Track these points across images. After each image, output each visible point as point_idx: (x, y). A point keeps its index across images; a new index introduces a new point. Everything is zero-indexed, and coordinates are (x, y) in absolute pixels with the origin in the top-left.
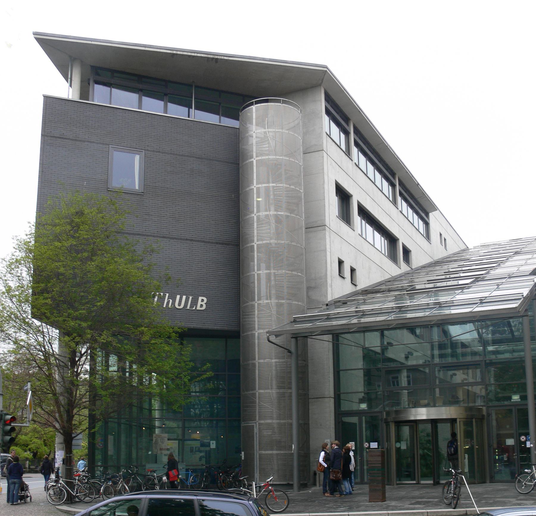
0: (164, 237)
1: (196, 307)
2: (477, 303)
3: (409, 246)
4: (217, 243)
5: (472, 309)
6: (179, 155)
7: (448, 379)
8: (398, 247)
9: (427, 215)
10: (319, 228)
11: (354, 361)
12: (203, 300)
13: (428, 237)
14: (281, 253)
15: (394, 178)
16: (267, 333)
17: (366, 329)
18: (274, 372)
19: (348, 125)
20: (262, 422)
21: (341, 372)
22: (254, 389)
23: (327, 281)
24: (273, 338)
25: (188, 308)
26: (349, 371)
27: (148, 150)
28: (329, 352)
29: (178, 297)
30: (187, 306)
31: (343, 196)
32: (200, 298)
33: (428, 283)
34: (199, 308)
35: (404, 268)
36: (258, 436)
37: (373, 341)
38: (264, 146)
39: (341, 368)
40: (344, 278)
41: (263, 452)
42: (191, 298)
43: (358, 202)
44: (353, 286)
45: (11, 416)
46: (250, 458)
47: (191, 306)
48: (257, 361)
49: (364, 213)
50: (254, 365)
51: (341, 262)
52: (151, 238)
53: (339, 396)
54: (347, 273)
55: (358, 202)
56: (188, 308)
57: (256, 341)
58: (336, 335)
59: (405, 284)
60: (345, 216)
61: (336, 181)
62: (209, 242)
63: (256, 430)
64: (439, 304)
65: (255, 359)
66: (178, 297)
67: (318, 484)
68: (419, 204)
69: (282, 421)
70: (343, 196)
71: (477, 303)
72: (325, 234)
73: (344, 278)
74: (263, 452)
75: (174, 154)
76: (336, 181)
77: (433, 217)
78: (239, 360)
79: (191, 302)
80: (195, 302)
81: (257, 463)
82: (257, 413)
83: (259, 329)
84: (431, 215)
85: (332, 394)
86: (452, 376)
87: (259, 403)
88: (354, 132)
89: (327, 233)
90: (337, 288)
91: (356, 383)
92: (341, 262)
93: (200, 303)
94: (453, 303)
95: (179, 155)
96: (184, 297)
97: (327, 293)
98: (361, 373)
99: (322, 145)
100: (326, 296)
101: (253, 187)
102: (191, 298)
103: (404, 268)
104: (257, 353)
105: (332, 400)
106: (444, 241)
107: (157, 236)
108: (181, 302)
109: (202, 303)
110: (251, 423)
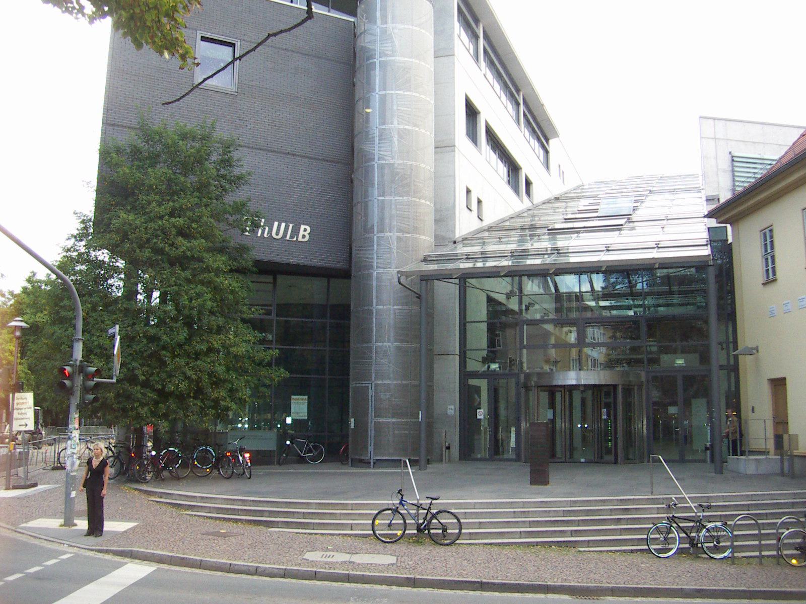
0: (260, 149)
1: (297, 237)
2: (603, 251)
3: (531, 178)
4: (324, 160)
5: (498, 262)
6: (282, 49)
7: (563, 337)
8: (520, 179)
9: (547, 140)
10: (448, 148)
11: (479, 311)
12: (305, 230)
13: (547, 166)
14: (406, 176)
15: (518, 94)
16: (398, 272)
17: (494, 273)
18: (392, 322)
19: (477, 27)
20: (379, 382)
21: (467, 324)
22: (370, 341)
23: (454, 213)
24: (403, 280)
25: (288, 238)
26: (473, 324)
27: (244, 40)
28: (455, 300)
29: (276, 224)
30: (286, 236)
31: (472, 112)
32: (303, 227)
33: (565, 222)
34: (300, 239)
35: (527, 203)
36: (373, 400)
37: (500, 288)
38: (387, 45)
39: (468, 320)
40: (470, 210)
41: (380, 420)
42: (291, 226)
43: (486, 122)
44: (479, 221)
45: (96, 369)
46: (362, 426)
47: (292, 237)
48: (375, 307)
49: (490, 134)
50: (370, 312)
51: (468, 191)
52: (245, 149)
53: (465, 352)
54: (474, 206)
55: (486, 122)
56: (288, 238)
57: (374, 283)
58: (464, 278)
59: (527, 221)
60: (472, 135)
61: (466, 96)
62: (315, 159)
63: (371, 393)
64: (557, 250)
65: (372, 305)
66: (276, 224)
67: (444, 460)
68: (540, 129)
69: (404, 382)
70: (472, 112)
71: (603, 251)
72: (454, 156)
73: (470, 210)
74: (380, 420)
75: (276, 48)
76: (466, 96)
77: (553, 144)
78: (349, 306)
79: (292, 232)
80: (296, 232)
81: (371, 432)
82: (373, 371)
83: (378, 267)
84: (551, 141)
85: (457, 352)
86: (566, 334)
87: (376, 359)
88: (484, 38)
89: (457, 156)
90: (465, 224)
91: (479, 337)
92: (468, 191)
93: (302, 233)
94: (568, 249)
95: (282, 49)
96: (283, 225)
97: (455, 228)
98: (484, 326)
99: (453, 49)
100: (453, 232)
101: (375, 94)
102: (291, 226)
103: (527, 203)
104: (374, 297)
105: (458, 357)
106: (562, 174)
107: (252, 148)
108: (279, 230)
109: (305, 231)
110: (365, 384)
